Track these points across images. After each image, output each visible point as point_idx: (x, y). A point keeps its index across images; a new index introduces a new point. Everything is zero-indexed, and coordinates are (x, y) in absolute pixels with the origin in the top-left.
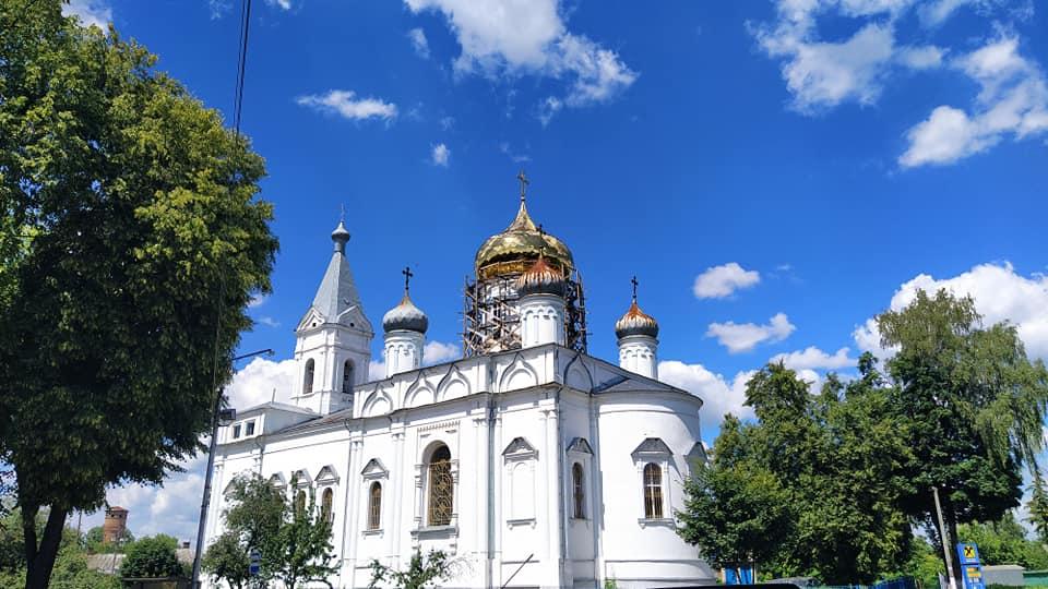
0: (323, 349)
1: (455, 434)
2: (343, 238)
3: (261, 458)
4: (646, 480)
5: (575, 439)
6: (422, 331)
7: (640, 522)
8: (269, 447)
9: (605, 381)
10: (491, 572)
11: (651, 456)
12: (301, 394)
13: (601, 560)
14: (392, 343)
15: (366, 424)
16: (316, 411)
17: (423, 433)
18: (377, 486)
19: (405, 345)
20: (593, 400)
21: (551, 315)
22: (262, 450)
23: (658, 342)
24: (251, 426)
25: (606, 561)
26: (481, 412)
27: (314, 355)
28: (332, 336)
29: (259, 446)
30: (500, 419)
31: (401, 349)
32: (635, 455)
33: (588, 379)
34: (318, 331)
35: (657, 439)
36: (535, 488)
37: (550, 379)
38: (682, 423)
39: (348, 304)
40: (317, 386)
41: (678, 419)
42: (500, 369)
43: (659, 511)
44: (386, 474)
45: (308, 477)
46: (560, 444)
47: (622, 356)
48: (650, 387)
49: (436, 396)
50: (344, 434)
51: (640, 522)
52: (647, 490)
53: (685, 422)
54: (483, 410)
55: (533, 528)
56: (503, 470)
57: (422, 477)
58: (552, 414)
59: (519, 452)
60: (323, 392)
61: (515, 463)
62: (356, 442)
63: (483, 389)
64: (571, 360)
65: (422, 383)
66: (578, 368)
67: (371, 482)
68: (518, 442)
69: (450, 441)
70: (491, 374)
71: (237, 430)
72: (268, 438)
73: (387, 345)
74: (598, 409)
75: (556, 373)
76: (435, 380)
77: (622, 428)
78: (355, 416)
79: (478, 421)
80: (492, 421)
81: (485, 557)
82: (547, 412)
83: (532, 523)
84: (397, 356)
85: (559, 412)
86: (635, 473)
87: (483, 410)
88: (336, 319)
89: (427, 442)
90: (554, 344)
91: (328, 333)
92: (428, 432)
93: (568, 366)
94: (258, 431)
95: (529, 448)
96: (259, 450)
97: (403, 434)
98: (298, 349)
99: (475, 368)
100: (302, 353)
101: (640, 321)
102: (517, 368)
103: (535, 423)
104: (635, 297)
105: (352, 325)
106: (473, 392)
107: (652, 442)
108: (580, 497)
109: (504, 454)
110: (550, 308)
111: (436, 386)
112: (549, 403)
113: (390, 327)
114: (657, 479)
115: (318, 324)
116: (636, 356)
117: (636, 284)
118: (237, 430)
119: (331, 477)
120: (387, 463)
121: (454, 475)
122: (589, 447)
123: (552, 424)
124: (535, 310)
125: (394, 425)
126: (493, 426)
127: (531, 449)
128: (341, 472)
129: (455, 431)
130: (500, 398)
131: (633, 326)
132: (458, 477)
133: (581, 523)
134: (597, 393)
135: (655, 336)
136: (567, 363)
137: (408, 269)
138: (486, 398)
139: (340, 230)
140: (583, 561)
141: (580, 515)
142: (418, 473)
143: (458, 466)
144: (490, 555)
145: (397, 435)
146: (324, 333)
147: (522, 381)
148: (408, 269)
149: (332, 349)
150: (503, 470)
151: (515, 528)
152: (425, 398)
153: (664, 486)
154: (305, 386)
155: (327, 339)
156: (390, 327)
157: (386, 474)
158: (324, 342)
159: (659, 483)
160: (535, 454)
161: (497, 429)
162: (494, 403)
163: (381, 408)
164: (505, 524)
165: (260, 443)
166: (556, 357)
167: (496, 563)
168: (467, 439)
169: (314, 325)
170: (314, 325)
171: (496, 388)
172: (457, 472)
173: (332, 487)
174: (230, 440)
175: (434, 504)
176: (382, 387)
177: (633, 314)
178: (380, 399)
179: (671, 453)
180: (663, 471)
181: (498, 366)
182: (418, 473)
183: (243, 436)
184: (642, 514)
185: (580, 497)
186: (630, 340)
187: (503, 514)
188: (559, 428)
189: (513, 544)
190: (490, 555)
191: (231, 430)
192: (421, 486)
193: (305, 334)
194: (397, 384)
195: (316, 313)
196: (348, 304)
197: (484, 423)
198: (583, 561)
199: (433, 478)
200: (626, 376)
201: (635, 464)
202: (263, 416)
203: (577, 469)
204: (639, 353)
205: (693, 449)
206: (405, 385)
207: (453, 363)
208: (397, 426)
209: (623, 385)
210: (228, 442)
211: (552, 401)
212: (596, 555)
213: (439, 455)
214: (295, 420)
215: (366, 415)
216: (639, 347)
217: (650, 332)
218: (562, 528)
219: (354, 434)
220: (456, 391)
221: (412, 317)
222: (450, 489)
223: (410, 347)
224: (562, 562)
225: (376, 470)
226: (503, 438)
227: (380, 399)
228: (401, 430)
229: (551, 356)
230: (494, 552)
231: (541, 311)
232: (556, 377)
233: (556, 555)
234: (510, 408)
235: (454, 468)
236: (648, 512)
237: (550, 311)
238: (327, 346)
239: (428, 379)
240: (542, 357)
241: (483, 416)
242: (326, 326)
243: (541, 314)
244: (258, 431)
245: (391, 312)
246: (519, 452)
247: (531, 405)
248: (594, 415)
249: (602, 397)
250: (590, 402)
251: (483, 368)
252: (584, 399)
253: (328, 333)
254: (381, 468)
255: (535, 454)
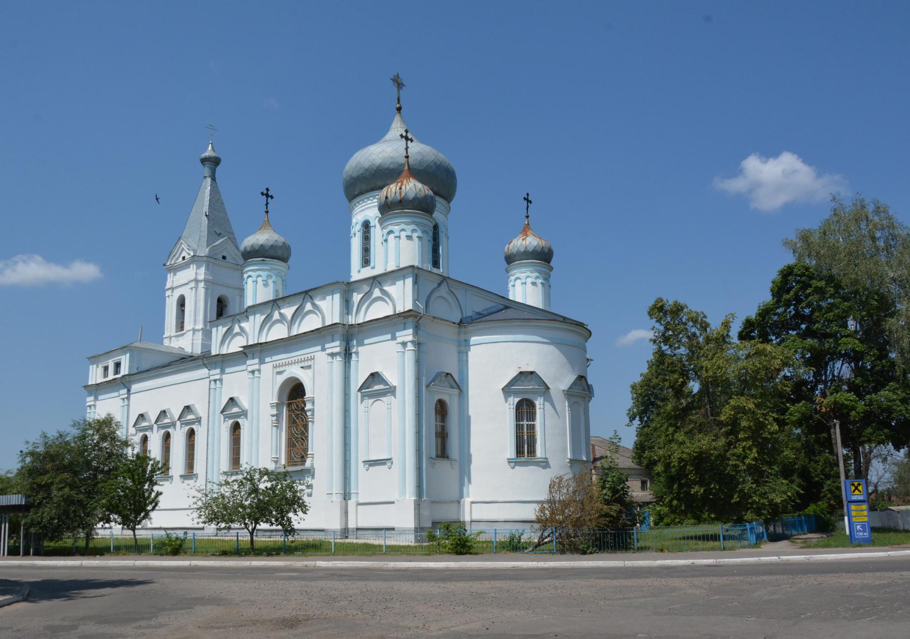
0: (193, 284)
1: (311, 370)
2: (214, 162)
3: (128, 398)
4: (519, 416)
5: (439, 374)
6: (284, 259)
7: (510, 461)
8: (135, 387)
9: (479, 310)
10: (346, 512)
11: (525, 396)
12: (174, 333)
13: (467, 501)
14: (250, 273)
15: (223, 361)
16: (188, 350)
17: (278, 370)
18: (236, 427)
19: (264, 274)
20: (463, 330)
21: (415, 235)
22: (129, 390)
23: (551, 269)
24: (118, 365)
25: (472, 503)
26: (335, 346)
27: (186, 291)
28: (202, 270)
29: (125, 387)
30: (357, 353)
31: (260, 279)
32: (507, 390)
33: (452, 309)
34: (185, 266)
35: (532, 373)
36: (392, 427)
37: (409, 306)
38: (562, 356)
39: (219, 235)
40: (188, 325)
41: (557, 352)
42: (356, 297)
43: (532, 451)
44: (198, 420)
45: (172, 417)
46: (418, 379)
47: (510, 285)
48: (526, 315)
49: (290, 329)
50: (204, 372)
51: (510, 461)
52: (519, 428)
53: (561, 351)
54: (337, 343)
55: (390, 468)
56: (361, 408)
57: (278, 416)
58: (410, 347)
59: (377, 387)
60: (194, 330)
61: (371, 401)
62: (215, 381)
63: (337, 320)
64: (436, 285)
65: (276, 316)
66: (445, 295)
67: (231, 421)
68: (375, 377)
69: (305, 377)
70: (347, 304)
71: (106, 369)
72: (133, 378)
73: (245, 276)
74: (467, 341)
75: (415, 300)
76: (288, 312)
77: (493, 361)
78: (213, 353)
79: (332, 355)
80: (347, 354)
81: (337, 499)
82: (404, 344)
83: (389, 464)
84: (257, 286)
85: (418, 344)
86: (507, 410)
87: (337, 343)
88: (204, 252)
89: (281, 379)
90: (413, 266)
91: (198, 268)
92: (281, 369)
93: (432, 292)
94: (124, 370)
95: (386, 383)
96: (125, 391)
97: (259, 370)
98: (168, 285)
99: (329, 298)
100: (172, 289)
101: (531, 242)
102: (374, 296)
103: (390, 357)
104: (527, 217)
105: (224, 258)
106: (328, 323)
107: (524, 376)
108: (441, 434)
109: (359, 390)
110: (413, 227)
111: (289, 318)
112: (407, 335)
113: (250, 255)
114: (532, 416)
115: (187, 257)
116: (399, 237)
117: (529, 201)
118: (106, 369)
119: (381, 387)
120: (245, 402)
121: (309, 413)
122: (457, 384)
123: (410, 356)
124: (396, 228)
125: (249, 362)
126: (349, 362)
127: (387, 384)
128: (201, 409)
129: (309, 367)
130: (356, 329)
131: (522, 250)
132: (313, 415)
133: (443, 464)
134: (469, 323)
135: (549, 262)
136: (430, 289)
137: (267, 190)
138: (340, 329)
139: (209, 152)
140: (440, 502)
141: (443, 453)
142: (275, 412)
143: (313, 403)
144: (346, 496)
145: (253, 372)
146: (193, 267)
147: (379, 310)
148: (267, 190)
149: (202, 285)
150: (361, 408)
151: (371, 468)
152: (278, 332)
153: (538, 423)
154: (177, 324)
155: (196, 274)
156: (250, 255)
157: (244, 413)
158: (193, 277)
159: (533, 419)
160: (391, 391)
161: (353, 363)
162: (348, 336)
163: (235, 345)
164: (361, 465)
165: (125, 383)
166: (415, 282)
167: (351, 504)
168: (320, 374)
169: (184, 258)
170: (184, 258)
171: (352, 320)
172: (313, 410)
173: (194, 427)
174: (100, 379)
175: (291, 444)
176: (239, 322)
177: (525, 230)
178: (237, 334)
179: (548, 388)
180: (538, 407)
181: (355, 294)
182: (275, 412)
183: (111, 376)
184: (511, 452)
185: (441, 434)
186: (520, 266)
187: (361, 452)
188: (418, 361)
189: (367, 484)
190: (346, 496)
191: (100, 370)
192: (278, 426)
193: (175, 269)
194: (251, 318)
195: (184, 246)
196: (219, 235)
197: (339, 358)
198: (440, 502)
199: (290, 417)
200: (508, 305)
201: (506, 401)
202: (128, 355)
203: (442, 409)
204: (529, 280)
205: (574, 384)
206: (259, 318)
207: (306, 292)
208: (252, 364)
209: (502, 314)
210: (98, 382)
211: (410, 331)
212: (461, 496)
213: (295, 393)
214: (166, 360)
215: (224, 351)
216: (529, 274)
217: (543, 257)
218: (419, 469)
219: (213, 372)
220: (311, 323)
221: (271, 243)
222: (306, 427)
223: (269, 277)
224: (418, 505)
225: (235, 410)
226: (359, 376)
227: (237, 334)
228: (256, 367)
229: (409, 281)
230: (350, 494)
231: (403, 230)
232: (414, 304)
233: (410, 497)
234: (366, 342)
235: (308, 406)
236: (519, 452)
237: (414, 231)
238: (197, 281)
239: (282, 311)
240: (400, 283)
241: (337, 350)
242: (195, 259)
243: (403, 234)
244: (124, 370)
245: (249, 238)
246: (377, 387)
247: (389, 336)
248: (464, 347)
249: (470, 328)
250: (459, 333)
251: (337, 297)
252: (450, 332)
253: (198, 268)
254: (240, 407)
255: (391, 391)
